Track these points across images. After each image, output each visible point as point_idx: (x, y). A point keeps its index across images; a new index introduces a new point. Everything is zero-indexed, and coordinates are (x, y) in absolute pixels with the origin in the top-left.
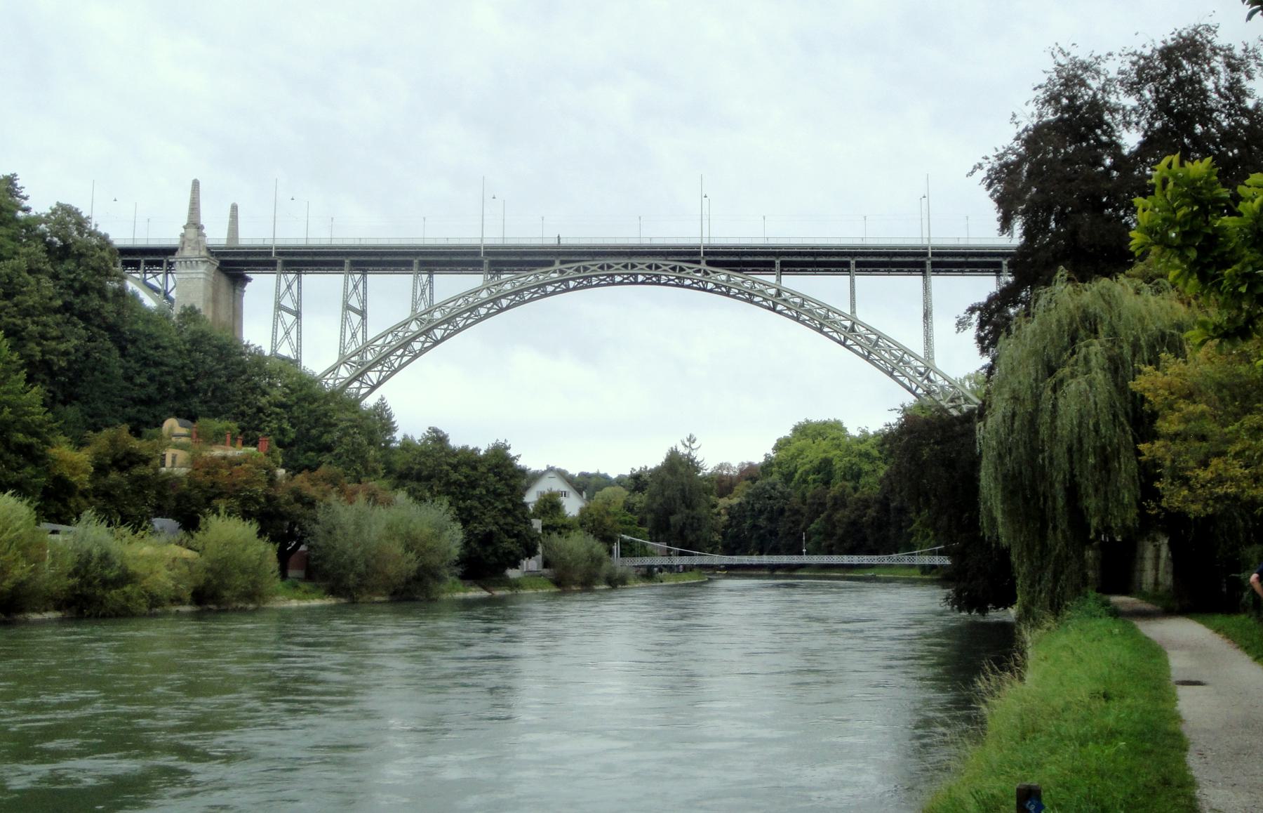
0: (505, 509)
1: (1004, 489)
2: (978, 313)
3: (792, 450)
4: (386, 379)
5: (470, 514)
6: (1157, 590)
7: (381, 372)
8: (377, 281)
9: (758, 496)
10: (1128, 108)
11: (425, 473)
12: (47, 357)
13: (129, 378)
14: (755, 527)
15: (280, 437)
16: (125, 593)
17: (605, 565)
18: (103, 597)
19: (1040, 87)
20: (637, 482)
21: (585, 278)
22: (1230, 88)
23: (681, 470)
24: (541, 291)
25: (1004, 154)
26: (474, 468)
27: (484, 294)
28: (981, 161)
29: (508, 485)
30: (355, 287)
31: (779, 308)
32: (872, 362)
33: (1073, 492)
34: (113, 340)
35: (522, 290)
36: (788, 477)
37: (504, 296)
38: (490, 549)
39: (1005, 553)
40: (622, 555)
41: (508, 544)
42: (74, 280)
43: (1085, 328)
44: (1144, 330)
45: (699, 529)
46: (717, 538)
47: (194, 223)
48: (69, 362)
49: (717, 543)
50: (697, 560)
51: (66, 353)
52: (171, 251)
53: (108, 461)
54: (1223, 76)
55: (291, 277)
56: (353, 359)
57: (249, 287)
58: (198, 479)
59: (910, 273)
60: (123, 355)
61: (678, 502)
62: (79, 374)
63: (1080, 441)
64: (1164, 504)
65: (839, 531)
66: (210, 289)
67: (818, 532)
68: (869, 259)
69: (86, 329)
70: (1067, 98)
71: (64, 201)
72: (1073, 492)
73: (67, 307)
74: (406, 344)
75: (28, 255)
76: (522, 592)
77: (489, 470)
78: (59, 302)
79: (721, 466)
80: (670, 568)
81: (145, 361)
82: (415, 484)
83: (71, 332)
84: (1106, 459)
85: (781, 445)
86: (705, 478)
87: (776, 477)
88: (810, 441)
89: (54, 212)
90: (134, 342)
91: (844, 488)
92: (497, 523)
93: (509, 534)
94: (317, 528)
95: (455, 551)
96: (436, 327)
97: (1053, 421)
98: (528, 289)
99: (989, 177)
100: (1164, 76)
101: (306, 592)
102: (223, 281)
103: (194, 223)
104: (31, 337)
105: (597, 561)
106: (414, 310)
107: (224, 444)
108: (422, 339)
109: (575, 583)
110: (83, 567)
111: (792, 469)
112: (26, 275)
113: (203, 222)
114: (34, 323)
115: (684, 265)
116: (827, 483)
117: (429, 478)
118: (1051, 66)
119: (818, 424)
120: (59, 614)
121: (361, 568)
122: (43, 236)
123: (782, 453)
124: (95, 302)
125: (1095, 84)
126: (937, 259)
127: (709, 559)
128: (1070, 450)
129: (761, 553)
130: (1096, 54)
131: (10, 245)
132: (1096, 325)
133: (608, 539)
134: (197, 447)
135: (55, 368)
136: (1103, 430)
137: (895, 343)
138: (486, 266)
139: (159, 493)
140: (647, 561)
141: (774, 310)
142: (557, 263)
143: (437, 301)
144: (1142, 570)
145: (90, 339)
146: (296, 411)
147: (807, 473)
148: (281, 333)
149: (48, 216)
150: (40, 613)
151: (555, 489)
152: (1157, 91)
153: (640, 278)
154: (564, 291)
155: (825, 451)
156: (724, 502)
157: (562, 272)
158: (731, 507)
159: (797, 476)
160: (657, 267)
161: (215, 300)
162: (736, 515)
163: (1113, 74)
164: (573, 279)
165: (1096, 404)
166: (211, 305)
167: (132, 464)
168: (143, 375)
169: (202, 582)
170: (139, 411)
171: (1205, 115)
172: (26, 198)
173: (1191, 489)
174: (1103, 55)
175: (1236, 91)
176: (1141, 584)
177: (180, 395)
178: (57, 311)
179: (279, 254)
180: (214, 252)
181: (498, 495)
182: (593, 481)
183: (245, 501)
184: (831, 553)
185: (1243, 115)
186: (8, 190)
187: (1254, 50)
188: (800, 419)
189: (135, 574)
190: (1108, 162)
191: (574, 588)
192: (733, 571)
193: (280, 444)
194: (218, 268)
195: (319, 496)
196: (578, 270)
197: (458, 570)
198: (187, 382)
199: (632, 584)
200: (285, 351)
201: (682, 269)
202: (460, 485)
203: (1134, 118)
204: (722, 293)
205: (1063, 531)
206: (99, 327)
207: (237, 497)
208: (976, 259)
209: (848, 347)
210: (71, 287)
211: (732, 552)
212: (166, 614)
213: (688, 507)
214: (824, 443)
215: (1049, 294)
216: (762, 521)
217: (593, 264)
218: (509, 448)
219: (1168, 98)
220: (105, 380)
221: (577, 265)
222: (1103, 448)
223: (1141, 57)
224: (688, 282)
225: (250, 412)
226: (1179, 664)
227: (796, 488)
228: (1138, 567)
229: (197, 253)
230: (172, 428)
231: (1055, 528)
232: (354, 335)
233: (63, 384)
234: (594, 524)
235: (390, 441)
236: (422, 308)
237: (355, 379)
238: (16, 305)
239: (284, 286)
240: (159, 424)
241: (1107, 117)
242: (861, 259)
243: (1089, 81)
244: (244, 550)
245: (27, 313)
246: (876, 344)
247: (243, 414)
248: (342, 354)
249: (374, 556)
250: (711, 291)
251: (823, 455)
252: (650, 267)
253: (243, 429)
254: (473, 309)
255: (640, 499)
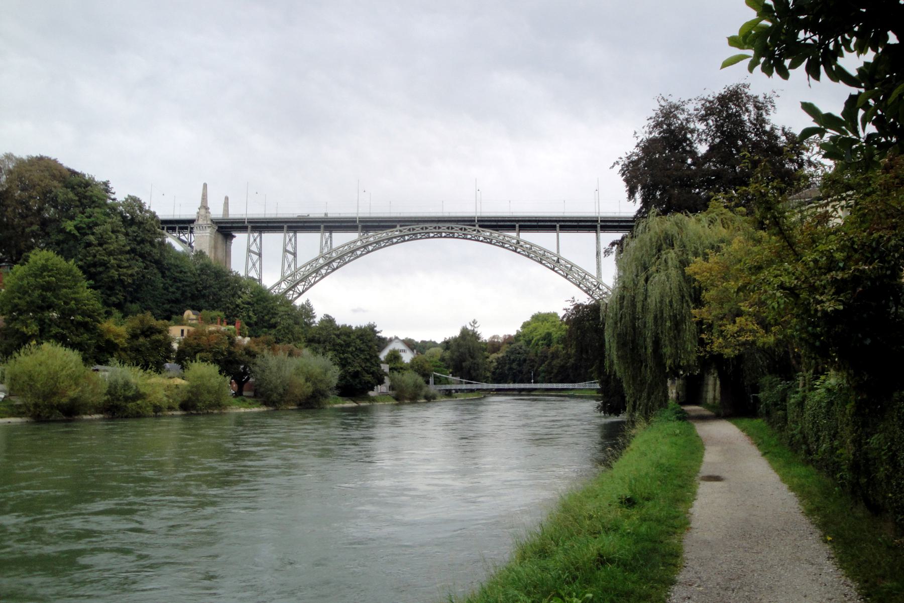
0: (366, 358)
1: (618, 343)
2: (616, 246)
3: (531, 328)
4: (307, 289)
5: (346, 361)
6: (714, 403)
7: (304, 285)
8: (302, 236)
9: (512, 352)
10: (701, 130)
11: (322, 339)
12: (122, 277)
13: (166, 289)
14: (511, 369)
15: (248, 320)
16: (138, 404)
17: (426, 389)
18: (126, 406)
19: (651, 118)
20: (447, 345)
21: (414, 234)
22: (757, 119)
23: (468, 338)
24: (390, 241)
25: (631, 156)
26: (349, 336)
27: (359, 244)
28: (618, 160)
29: (367, 346)
30: (290, 240)
31: (519, 250)
32: (568, 279)
33: (657, 343)
34: (158, 268)
35: (380, 241)
36: (529, 342)
37: (370, 244)
38: (357, 380)
39: (619, 382)
40: (435, 384)
41: (368, 378)
42: (137, 236)
43: (666, 243)
44: (701, 244)
45: (478, 369)
46: (489, 374)
47: (204, 206)
48: (134, 280)
49: (488, 377)
50: (474, 387)
51: (132, 275)
52: (192, 221)
53: (139, 332)
54: (753, 113)
55: (256, 235)
56: (289, 278)
57: (234, 240)
58: (190, 342)
59: (589, 231)
60: (163, 277)
61: (467, 355)
62: (139, 287)
63: (662, 312)
64: (708, 349)
65: (555, 371)
66: (213, 242)
67: (543, 371)
68: (567, 224)
69: (143, 262)
70: (666, 124)
71: (132, 194)
72: (657, 343)
73: (133, 251)
74: (317, 271)
75: (112, 223)
76: (376, 403)
77: (357, 338)
78: (128, 248)
79: (494, 337)
80: (462, 391)
81: (175, 280)
82: (316, 345)
83: (135, 265)
84: (677, 324)
85: (525, 325)
86: (482, 342)
87: (522, 342)
88: (540, 323)
89: (127, 200)
90: (169, 269)
91: (558, 347)
92: (361, 366)
93: (368, 372)
94: (257, 369)
95: (335, 381)
96: (334, 261)
97: (646, 299)
98: (383, 240)
99: (622, 169)
100: (721, 111)
101: (250, 404)
102: (220, 237)
103: (204, 206)
104: (113, 266)
105: (420, 387)
106: (321, 252)
107: (217, 324)
108: (326, 268)
109: (407, 399)
110: (112, 390)
111: (531, 338)
112: (110, 233)
113: (209, 205)
114: (115, 259)
115: (467, 227)
116: (549, 345)
117: (325, 341)
118: (657, 107)
119: (545, 314)
120: (101, 416)
121: (281, 390)
122: (121, 213)
123: (526, 330)
124: (148, 247)
125: (681, 117)
126: (603, 224)
127: (485, 386)
128: (655, 317)
129: (514, 382)
130: (682, 100)
131: (102, 218)
132: (672, 241)
133: (425, 375)
134: (200, 326)
135: (126, 283)
136: (675, 305)
137: (581, 269)
138: (360, 228)
139: (166, 349)
140: (448, 387)
141: (515, 251)
142: (398, 226)
143: (334, 246)
144: (707, 391)
145: (145, 268)
146: (256, 307)
147: (539, 340)
148: (250, 265)
149: (123, 202)
150: (90, 415)
151: (397, 348)
152: (716, 121)
153: (444, 234)
154: (402, 242)
155: (548, 329)
156: (495, 355)
157: (401, 231)
158: (498, 358)
159: (533, 342)
160: (452, 228)
161: (215, 248)
162: (501, 362)
163: (692, 111)
164: (408, 235)
165: (671, 289)
166: (213, 250)
167: (152, 333)
168: (174, 287)
169: (185, 398)
170: (171, 307)
171: (743, 136)
172: (114, 194)
173: (724, 337)
174: (686, 100)
175: (760, 121)
176: (706, 399)
177: (194, 297)
178: (128, 252)
179: (249, 222)
180: (215, 222)
181: (362, 351)
182: (428, 345)
183: (215, 354)
184: (550, 382)
185: (764, 135)
186: (104, 189)
187: (770, 98)
188: (535, 311)
189: (145, 394)
190: (689, 161)
191: (406, 401)
192: (499, 392)
193: (248, 324)
194: (218, 230)
195: (259, 351)
196: (409, 230)
197: (336, 392)
198: (198, 291)
199: (439, 399)
200: (253, 274)
201: (465, 230)
202: (341, 346)
203: (704, 137)
204: (487, 242)
205: (651, 368)
206: (151, 261)
207: (210, 352)
208: (624, 224)
209: (556, 271)
210: (135, 240)
211: (499, 382)
212: (164, 416)
213: (472, 358)
214: (547, 324)
215: (644, 223)
216: (514, 366)
217: (418, 228)
218: (375, 327)
219: (722, 125)
220: (153, 290)
221: (409, 227)
222: (675, 316)
223: (707, 100)
224: (469, 237)
225: (231, 307)
226: (711, 459)
227: (533, 347)
228: (705, 389)
229: (205, 222)
230: (189, 315)
231: (646, 366)
232: (289, 266)
233: (131, 292)
234: (418, 368)
235: (312, 323)
236: (325, 251)
237: (290, 289)
238: (105, 250)
239: (252, 240)
240: (182, 313)
241: (689, 136)
242: (563, 224)
243: (679, 115)
244: (209, 380)
245: (110, 254)
246: (571, 270)
247: (228, 308)
248: (283, 275)
249: (288, 385)
250: (482, 241)
251: (546, 331)
252: (448, 228)
253: (227, 317)
254: (353, 252)
255: (447, 354)
